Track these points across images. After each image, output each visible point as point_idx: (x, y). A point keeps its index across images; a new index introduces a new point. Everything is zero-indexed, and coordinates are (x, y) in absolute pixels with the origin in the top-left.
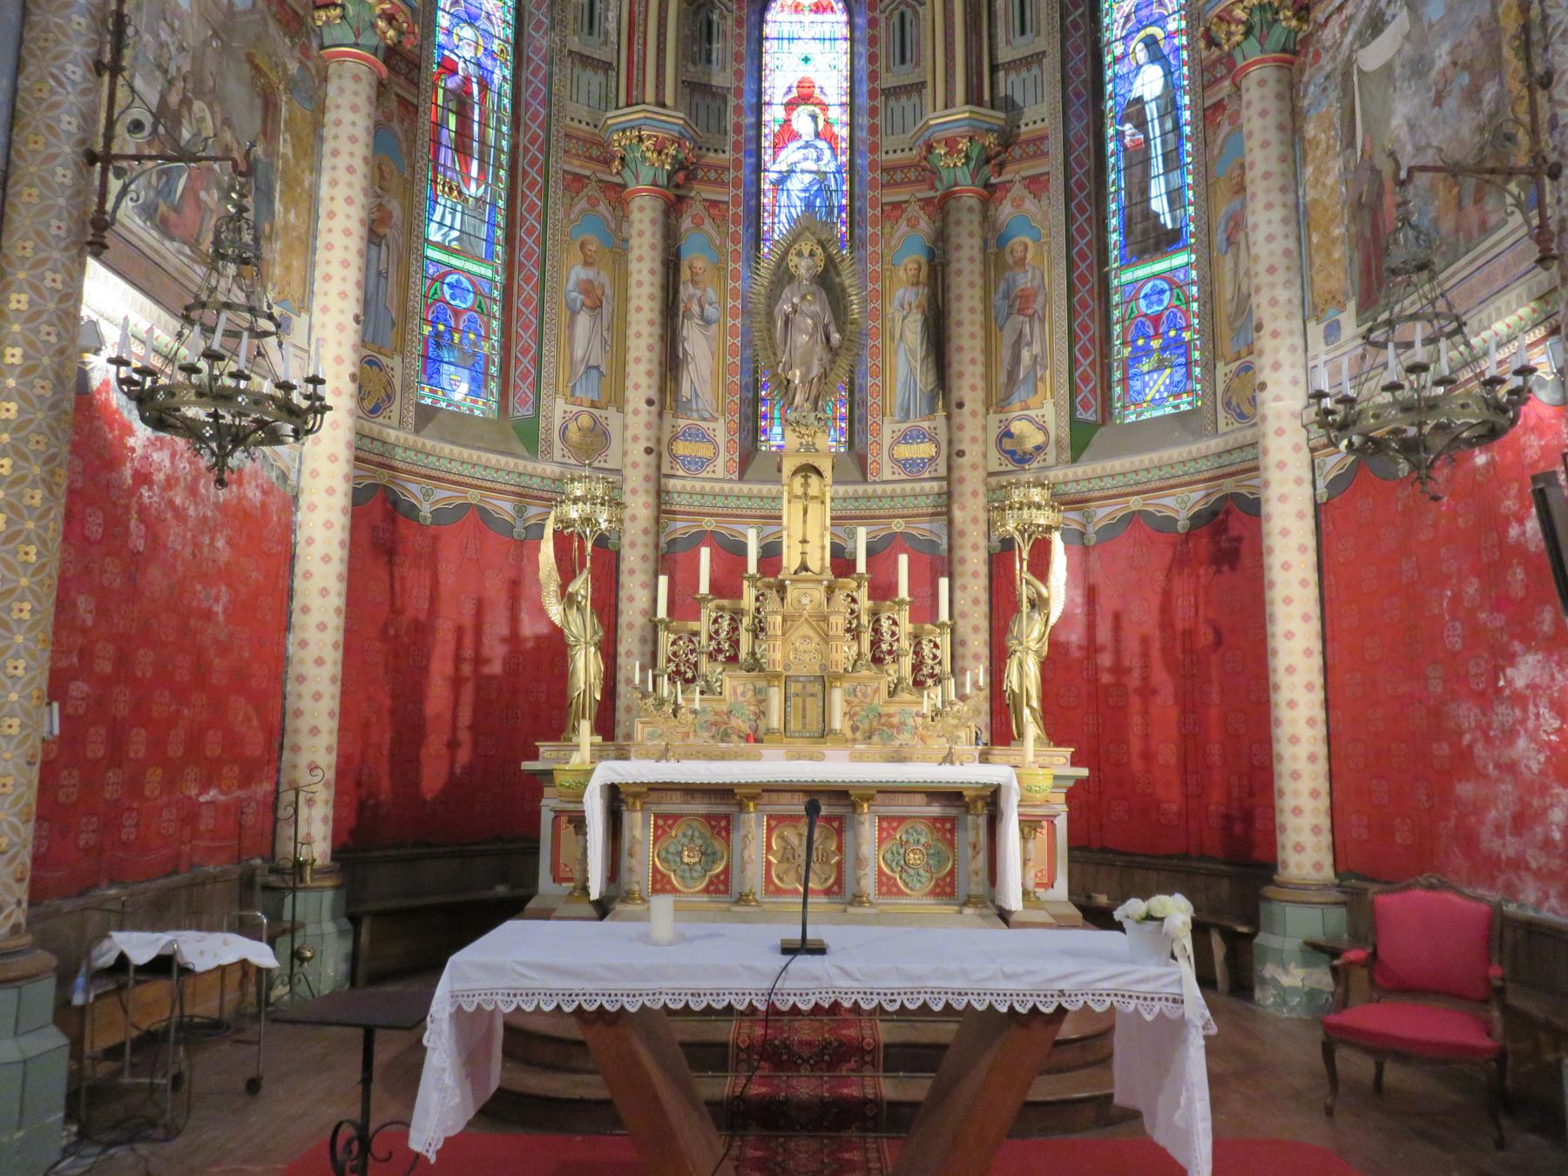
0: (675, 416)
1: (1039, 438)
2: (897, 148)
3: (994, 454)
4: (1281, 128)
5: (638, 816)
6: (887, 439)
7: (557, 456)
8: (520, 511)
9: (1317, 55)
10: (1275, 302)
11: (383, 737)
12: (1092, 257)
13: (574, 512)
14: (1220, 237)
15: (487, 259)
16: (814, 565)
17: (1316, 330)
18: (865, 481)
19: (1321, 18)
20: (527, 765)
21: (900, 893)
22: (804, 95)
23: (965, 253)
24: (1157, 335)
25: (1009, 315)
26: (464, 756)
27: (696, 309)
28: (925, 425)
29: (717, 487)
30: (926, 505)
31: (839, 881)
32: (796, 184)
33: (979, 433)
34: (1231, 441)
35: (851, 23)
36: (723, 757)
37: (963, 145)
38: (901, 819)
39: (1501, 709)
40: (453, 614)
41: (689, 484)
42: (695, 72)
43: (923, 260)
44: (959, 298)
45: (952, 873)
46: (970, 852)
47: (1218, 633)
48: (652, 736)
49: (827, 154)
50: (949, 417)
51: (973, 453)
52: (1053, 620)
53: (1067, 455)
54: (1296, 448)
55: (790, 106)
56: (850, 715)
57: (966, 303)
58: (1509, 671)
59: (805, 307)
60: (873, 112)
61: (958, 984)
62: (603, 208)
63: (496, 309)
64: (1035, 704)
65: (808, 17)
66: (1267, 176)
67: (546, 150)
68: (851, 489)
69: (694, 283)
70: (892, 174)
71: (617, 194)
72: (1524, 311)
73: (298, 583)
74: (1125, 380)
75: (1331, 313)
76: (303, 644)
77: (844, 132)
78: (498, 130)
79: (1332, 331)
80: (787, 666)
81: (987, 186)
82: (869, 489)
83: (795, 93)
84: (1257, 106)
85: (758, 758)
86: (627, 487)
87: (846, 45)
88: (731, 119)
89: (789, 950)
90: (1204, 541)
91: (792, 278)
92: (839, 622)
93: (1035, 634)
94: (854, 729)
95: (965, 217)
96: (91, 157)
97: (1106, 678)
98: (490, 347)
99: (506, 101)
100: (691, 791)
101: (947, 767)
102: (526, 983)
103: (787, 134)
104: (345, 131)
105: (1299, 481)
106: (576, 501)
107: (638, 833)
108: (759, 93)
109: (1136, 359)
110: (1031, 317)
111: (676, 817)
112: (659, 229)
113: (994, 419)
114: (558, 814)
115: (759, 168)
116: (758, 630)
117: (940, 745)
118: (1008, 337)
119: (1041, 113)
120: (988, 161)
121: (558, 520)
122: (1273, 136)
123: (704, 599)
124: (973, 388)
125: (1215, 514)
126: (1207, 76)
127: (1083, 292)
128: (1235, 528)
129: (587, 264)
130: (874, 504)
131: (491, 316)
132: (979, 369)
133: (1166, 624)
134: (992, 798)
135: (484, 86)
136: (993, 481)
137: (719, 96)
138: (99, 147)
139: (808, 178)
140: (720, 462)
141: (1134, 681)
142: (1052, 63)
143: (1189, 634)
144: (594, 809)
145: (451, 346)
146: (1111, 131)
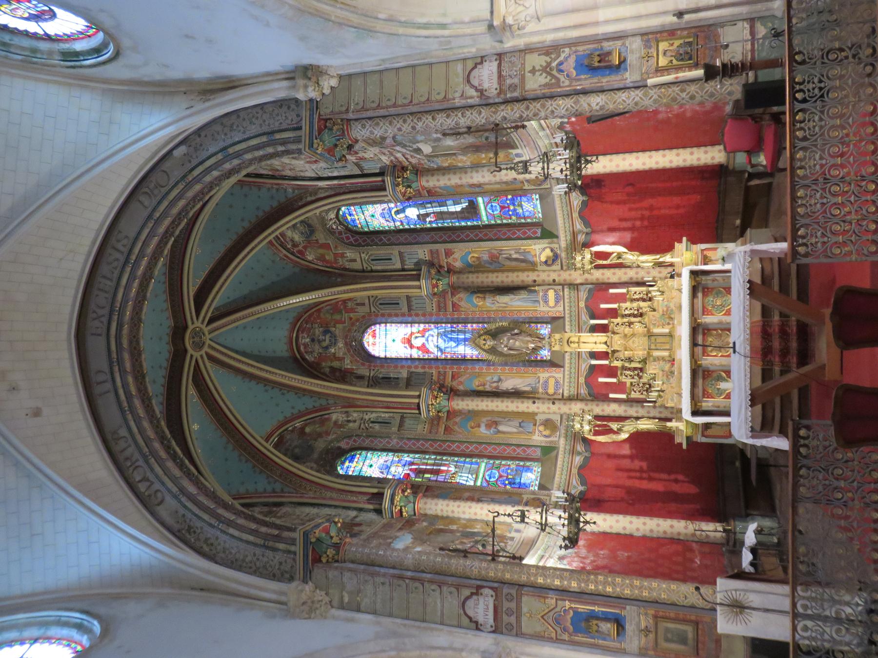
0: (538, 393)
2: (431, 306)
3: (554, 267)
4: (444, 174)
5: (704, 404)
6: (547, 309)
7: (556, 439)
8: (579, 454)
11: (673, 506)
12: (477, 232)
13: (587, 428)
15: (478, 464)
16: (604, 339)
18: (564, 318)
20: (684, 446)
23: (475, 280)
24: (508, 207)
26: (681, 477)
27: (495, 385)
28: (541, 294)
29: (567, 377)
30: (574, 294)
33: (546, 274)
35: (380, 323)
36: (680, 373)
37: (434, 282)
38: (704, 307)
40: (623, 480)
41: (566, 388)
42: (402, 384)
43: (476, 295)
44: (492, 282)
46: (716, 282)
47: (628, 185)
48: (672, 400)
49: (431, 332)
50: (539, 285)
51: (554, 276)
52: (625, 250)
53: (555, 240)
55: (412, 347)
56: (663, 326)
57: (494, 279)
59: (505, 343)
60: (417, 315)
62: (458, 419)
63: (497, 462)
64: (658, 257)
66: (460, 179)
67: (435, 441)
68: (567, 323)
69: (484, 385)
70: (441, 307)
71: (451, 414)
73: (614, 531)
74: (525, 218)
76: (638, 529)
77: (422, 326)
80: (645, 349)
82: (567, 316)
83: (407, 345)
85: (680, 360)
86: (568, 412)
88: (420, 370)
89: (734, 352)
90: (592, 191)
91: (493, 347)
92: (627, 330)
93: (631, 257)
94: (669, 324)
96: (493, 560)
97: (646, 223)
98: (513, 464)
99: (417, 456)
100: (694, 385)
101: (683, 291)
103: (423, 348)
104: (445, 508)
106: (582, 427)
107: (710, 404)
108: (406, 359)
109: (517, 215)
111: (704, 390)
112: (465, 398)
113: (539, 268)
114: (703, 435)
115: (436, 360)
116: (630, 360)
117: (675, 293)
118: (508, 263)
119: (422, 252)
121: (589, 434)
122: (447, 177)
123: (619, 380)
124: (528, 276)
127: (491, 235)
129: (479, 426)
130: (573, 314)
132: (520, 274)
133: (624, 202)
134: (693, 273)
135: (411, 464)
136: (565, 268)
137: (411, 374)
138: (490, 558)
139: (440, 340)
141: (647, 213)
142: (403, 249)
143: (628, 194)
144: (701, 420)
145: (514, 479)
146: (429, 226)
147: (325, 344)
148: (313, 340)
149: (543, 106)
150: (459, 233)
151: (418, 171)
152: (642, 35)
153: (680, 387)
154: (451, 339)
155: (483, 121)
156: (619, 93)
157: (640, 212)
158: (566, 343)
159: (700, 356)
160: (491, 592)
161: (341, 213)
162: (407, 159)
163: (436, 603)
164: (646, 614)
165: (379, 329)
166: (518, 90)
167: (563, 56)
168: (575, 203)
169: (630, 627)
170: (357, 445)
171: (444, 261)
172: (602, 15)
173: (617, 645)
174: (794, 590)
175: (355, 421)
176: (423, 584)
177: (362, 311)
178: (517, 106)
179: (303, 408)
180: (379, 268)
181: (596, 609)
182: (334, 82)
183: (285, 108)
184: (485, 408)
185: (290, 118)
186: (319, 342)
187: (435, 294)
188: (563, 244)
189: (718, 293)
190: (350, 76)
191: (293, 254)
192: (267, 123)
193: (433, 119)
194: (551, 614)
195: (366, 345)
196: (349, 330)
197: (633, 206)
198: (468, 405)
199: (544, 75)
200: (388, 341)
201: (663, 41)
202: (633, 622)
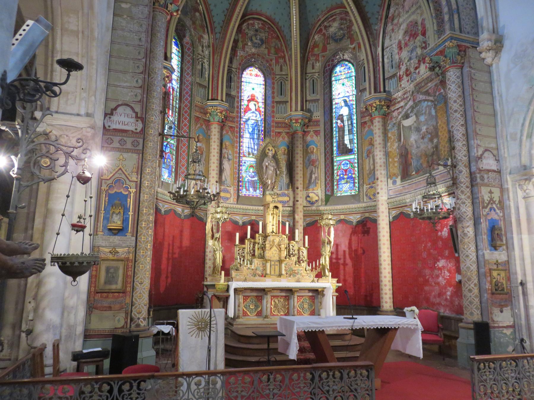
1: (317, 198)
2: (278, 117)
3: (305, 201)
4: (383, 133)
8: (183, 211)
9: (391, 118)
10: (381, 173)
14: (365, 155)
17: (390, 182)
19: (393, 110)
21: (302, 315)
22: (252, 99)
24: (346, 174)
25: (309, 166)
26: (169, 280)
28: (286, 192)
29: (232, 206)
31: (288, 312)
32: (251, 122)
34: (368, 204)
35: (265, 81)
38: (302, 296)
39: (436, 271)
43: (286, 148)
44: (297, 160)
45: (314, 309)
47: (364, 251)
49: (258, 115)
53: (324, 203)
54: (386, 208)
55: (249, 101)
56: (286, 270)
58: (438, 263)
59: (271, 164)
61: (382, 323)
62: (204, 127)
63: (174, 152)
64: (328, 268)
65: (254, 77)
66: (380, 144)
69: (226, 149)
71: (208, 123)
72: (443, 189)
74: (338, 185)
75: (394, 178)
77: (263, 110)
78: (176, 102)
79: (394, 183)
81: (304, 131)
83: (250, 98)
84: (377, 127)
87: (264, 87)
90: (360, 228)
94: (287, 274)
95: (299, 140)
98: (173, 163)
99: (178, 94)
102: (309, 326)
103: (248, 109)
105: (386, 216)
110: (315, 167)
111: (249, 296)
119: (318, 115)
120: (305, 125)
125: (363, 221)
126: (362, 115)
128: (368, 225)
131: (173, 155)
132: (302, 179)
136: (305, 208)
139: (253, 121)
140: (232, 199)
141: (341, 261)
142: (321, 102)
143: (356, 251)
146: (334, 121)
147: (254, 38)
148: (256, 31)
149: (468, 197)
150: (329, 141)
151: (386, 117)
152: (508, 261)
153: (250, 281)
154: (254, 129)
155: (459, 158)
156: (474, 246)
157: (342, 257)
158: (275, 205)
159: (244, 294)
160: (139, 129)
161: (347, 63)
162: (398, 109)
163: (126, 82)
164: (129, 252)
165: (261, 79)
166: (481, 182)
167: (498, 211)
168: (351, 217)
169: (116, 239)
170: (186, 50)
171: (311, 129)
172: (525, 237)
173: (101, 228)
174: (223, 373)
175: (203, 51)
176: (142, 73)
177: (277, 69)
178: (468, 180)
179: (213, 13)
180: (308, 85)
181: (131, 213)
182: (488, 61)
183: (472, 25)
184: (212, 147)
185: (467, 27)
186: (256, 35)
187: (291, 120)
188: (322, 208)
189: (311, 306)
190: (490, 73)
191: (320, 25)
192: (465, 10)
193: (462, 125)
194: (123, 176)
195: (250, 69)
196: (263, 58)
197: (347, 253)
198: (215, 135)
199: (489, 199)
200: (253, 83)
201: (505, 273)
202: (121, 242)
